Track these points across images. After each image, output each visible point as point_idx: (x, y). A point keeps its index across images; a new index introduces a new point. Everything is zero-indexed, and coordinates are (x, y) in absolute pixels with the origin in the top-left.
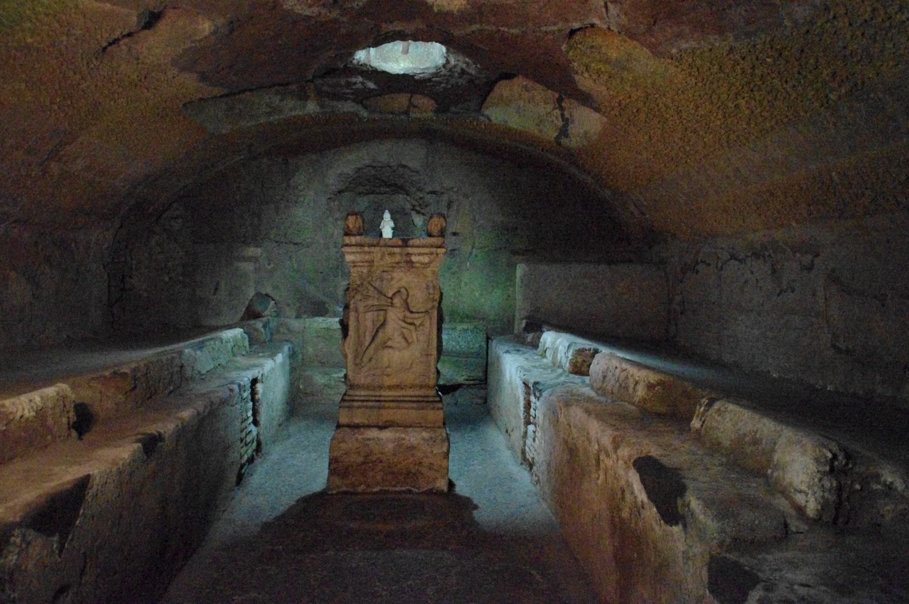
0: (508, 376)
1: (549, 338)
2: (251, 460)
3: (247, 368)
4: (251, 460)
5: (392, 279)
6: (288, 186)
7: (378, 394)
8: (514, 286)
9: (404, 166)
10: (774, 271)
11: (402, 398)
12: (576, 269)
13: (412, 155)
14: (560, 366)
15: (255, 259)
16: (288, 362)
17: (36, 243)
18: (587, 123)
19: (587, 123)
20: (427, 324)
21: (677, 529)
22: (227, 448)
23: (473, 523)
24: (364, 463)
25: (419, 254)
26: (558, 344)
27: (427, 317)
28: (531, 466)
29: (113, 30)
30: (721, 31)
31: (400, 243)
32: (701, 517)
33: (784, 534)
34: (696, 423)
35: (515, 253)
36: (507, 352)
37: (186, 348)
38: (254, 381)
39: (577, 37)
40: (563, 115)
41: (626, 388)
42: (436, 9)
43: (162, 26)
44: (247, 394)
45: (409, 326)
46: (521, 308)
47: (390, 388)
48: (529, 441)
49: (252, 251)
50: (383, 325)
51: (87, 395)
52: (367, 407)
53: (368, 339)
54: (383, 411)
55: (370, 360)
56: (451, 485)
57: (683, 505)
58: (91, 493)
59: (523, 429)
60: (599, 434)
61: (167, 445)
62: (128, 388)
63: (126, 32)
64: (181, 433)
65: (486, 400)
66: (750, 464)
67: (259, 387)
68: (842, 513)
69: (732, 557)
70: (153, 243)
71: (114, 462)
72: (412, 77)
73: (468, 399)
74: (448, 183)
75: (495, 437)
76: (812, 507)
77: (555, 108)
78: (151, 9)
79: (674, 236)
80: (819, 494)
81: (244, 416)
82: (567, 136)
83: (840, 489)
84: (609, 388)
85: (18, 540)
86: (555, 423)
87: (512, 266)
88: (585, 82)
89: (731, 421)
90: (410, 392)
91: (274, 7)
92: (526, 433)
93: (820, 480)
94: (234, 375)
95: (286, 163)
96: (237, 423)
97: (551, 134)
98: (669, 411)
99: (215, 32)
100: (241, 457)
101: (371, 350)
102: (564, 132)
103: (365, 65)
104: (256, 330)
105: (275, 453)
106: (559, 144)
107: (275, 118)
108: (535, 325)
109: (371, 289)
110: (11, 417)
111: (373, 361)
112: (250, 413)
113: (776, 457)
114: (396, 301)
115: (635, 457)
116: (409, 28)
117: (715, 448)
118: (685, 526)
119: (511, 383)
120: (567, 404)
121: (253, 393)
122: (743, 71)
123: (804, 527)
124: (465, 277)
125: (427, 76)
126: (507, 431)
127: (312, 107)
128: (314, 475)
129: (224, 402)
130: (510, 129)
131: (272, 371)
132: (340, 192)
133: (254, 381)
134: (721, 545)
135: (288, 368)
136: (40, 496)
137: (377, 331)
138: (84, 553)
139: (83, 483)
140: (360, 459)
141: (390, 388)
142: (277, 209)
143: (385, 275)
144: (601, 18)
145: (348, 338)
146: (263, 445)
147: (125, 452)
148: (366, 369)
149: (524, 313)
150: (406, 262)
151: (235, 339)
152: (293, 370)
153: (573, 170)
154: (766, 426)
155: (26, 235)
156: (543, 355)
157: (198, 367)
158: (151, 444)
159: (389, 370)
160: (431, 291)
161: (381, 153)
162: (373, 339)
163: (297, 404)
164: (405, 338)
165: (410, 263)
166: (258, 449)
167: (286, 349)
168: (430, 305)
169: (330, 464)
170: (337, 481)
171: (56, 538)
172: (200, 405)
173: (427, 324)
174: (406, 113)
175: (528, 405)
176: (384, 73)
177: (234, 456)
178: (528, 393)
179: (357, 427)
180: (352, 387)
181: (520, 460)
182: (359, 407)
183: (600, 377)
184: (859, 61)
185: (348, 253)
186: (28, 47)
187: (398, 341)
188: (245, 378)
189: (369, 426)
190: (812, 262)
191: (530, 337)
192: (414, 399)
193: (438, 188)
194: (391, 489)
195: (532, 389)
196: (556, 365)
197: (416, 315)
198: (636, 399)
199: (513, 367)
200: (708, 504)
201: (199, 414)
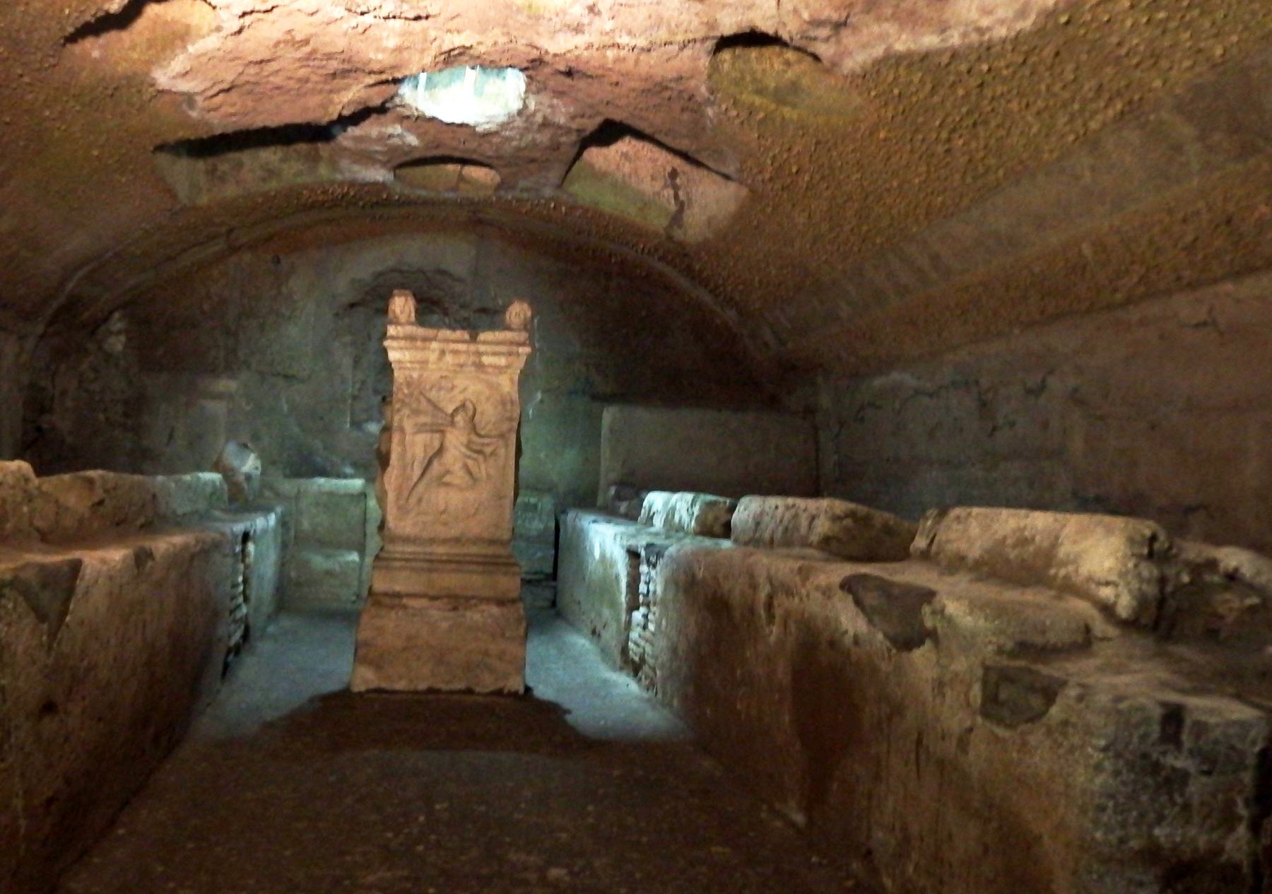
0: (597, 554)
1: (656, 500)
5: (453, 388)
6: (280, 293)
8: (598, 445)
15: (228, 397)
20: (502, 451)
24: (405, 649)
25: (495, 354)
27: (501, 442)
33: (1085, 642)
36: (594, 521)
40: (676, 196)
45: (475, 455)
46: (609, 468)
49: (226, 385)
50: (440, 451)
52: (413, 569)
53: (417, 472)
54: (435, 576)
55: (420, 501)
58: (81, 586)
70: (84, 366)
77: (665, 186)
80: (1135, 585)
82: (680, 226)
83: (1162, 581)
84: (767, 535)
92: (629, 623)
93: (1136, 566)
95: (277, 261)
101: (421, 488)
106: (670, 238)
107: (273, 185)
109: (422, 399)
111: (424, 504)
113: (1062, 552)
114: (459, 419)
123: (1112, 631)
125: (491, 127)
126: (594, 632)
130: (602, 215)
132: (352, 305)
133: (246, 537)
134: (1000, 651)
137: (430, 462)
140: (399, 643)
142: (262, 328)
148: (412, 515)
149: (613, 476)
150: (474, 364)
154: (1040, 521)
156: (650, 519)
158: (142, 557)
159: (444, 516)
160: (509, 407)
162: (423, 474)
164: (470, 473)
165: (480, 366)
166: (246, 636)
168: (505, 427)
180: (394, 539)
184: (1137, 65)
185: (394, 349)
187: (458, 476)
190: (1044, 381)
191: (623, 507)
197: (486, 441)
198: (814, 538)
199: (605, 540)
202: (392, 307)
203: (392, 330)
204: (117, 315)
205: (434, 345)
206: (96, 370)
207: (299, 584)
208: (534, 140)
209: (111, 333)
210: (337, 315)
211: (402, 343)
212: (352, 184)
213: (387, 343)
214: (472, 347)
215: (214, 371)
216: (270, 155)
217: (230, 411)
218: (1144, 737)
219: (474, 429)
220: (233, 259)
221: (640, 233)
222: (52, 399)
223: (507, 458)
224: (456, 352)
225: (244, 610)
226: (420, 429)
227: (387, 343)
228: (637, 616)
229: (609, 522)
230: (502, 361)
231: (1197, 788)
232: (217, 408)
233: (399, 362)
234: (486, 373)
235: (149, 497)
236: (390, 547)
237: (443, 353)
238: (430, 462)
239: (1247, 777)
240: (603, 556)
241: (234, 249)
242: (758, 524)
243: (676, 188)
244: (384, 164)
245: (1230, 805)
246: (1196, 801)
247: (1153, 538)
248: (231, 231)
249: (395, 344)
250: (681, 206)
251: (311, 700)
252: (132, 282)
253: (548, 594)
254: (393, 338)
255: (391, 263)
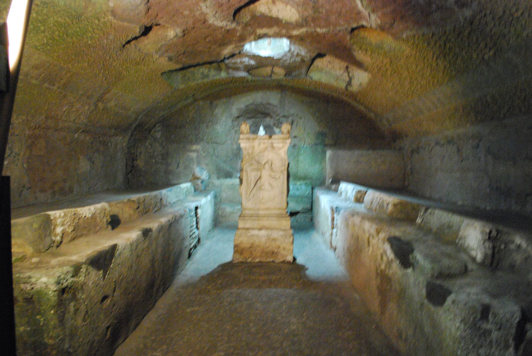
1: (343, 186)
2: (195, 247)
3: (193, 201)
4: (195, 247)
9: (270, 104)
10: (459, 150)
12: (357, 152)
13: (273, 98)
14: (349, 199)
16: (213, 200)
17: (92, 143)
18: (361, 78)
19: (361, 78)
21: (410, 270)
22: (184, 239)
23: (305, 276)
26: (348, 189)
28: (335, 249)
29: (128, 36)
30: (429, 25)
32: (422, 263)
33: (465, 271)
34: (419, 220)
35: (325, 145)
37: (164, 192)
38: (196, 208)
39: (356, 32)
41: (383, 206)
42: (284, 22)
43: (151, 34)
44: (193, 213)
47: (264, 209)
48: (334, 237)
49: (194, 147)
50: (260, 178)
51: (116, 211)
56: (295, 259)
57: (413, 259)
58: (117, 253)
60: (369, 227)
61: (154, 234)
62: (136, 207)
63: (134, 36)
64: (161, 228)
65: (312, 220)
66: (448, 239)
67: (199, 211)
68: (495, 260)
69: (438, 282)
70: (147, 144)
71: (128, 239)
72: (273, 58)
73: (303, 219)
74: (292, 111)
75: (316, 236)
76: (479, 257)
78: (146, 24)
79: (406, 136)
80: (483, 250)
81: (192, 224)
83: (494, 248)
84: (374, 207)
85: (84, 271)
86: (347, 225)
87: (324, 153)
88: (359, 55)
89: (438, 217)
91: (205, 22)
94: (187, 204)
96: (189, 229)
97: (343, 85)
98: (405, 216)
99: (176, 36)
100: (190, 245)
102: (349, 83)
103: (249, 52)
104: (197, 184)
105: (206, 244)
107: (206, 80)
108: (336, 181)
110: (80, 216)
112: (195, 223)
113: (461, 233)
115: (387, 237)
116: (271, 31)
117: (429, 231)
118: (414, 269)
119: (324, 208)
120: (353, 215)
121: (196, 214)
122: (440, 46)
124: (301, 158)
127: (223, 75)
128: (227, 255)
129: (181, 216)
131: (205, 203)
132: (238, 117)
133: (196, 208)
134: (432, 276)
135: (213, 204)
136: (94, 252)
137: (257, 182)
138: (115, 281)
139: (114, 247)
141: (264, 209)
142: (207, 126)
144: (367, 21)
145: (243, 185)
146: (201, 240)
147: (134, 235)
151: (187, 188)
152: (215, 204)
153: (354, 104)
154: (456, 219)
155: (88, 138)
157: (169, 200)
158: (146, 233)
161: (257, 98)
163: (218, 222)
167: (212, 193)
169: (234, 248)
170: (238, 256)
171: (101, 272)
172: (170, 217)
173: (282, 177)
174: (271, 76)
175: (333, 219)
176: (258, 56)
177: (187, 243)
178: (333, 214)
179: (248, 229)
181: (329, 246)
183: (370, 202)
186: (89, 45)
188: (193, 206)
189: (253, 229)
191: (334, 187)
193: (286, 114)
195: (335, 210)
196: (346, 199)
199: (325, 201)
200: (426, 256)
201: (169, 221)
202: (241, 128)
204: (157, 125)
206: (151, 145)
207: (222, 217)
208: (295, 61)
209: (156, 132)
210: (232, 121)
212: (233, 77)
215: (192, 143)
216: (204, 70)
217: (197, 156)
218: (474, 318)
219: (272, 169)
220: (196, 103)
221: (336, 90)
222: (137, 155)
223: (283, 182)
224: (264, 143)
225: (197, 233)
228: (335, 230)
229: (327, 194)
230: (281, 145)
231: (495, 335)
232: (194, 155)
235: (159, 200)
236: (244, 212)
237: (260, 144)
239: (514, 331)
240: (324, 206)
241: (196, 100)
242: (372, 203)
243: (349, 73)
244: (244, 70)
245: (507, 341)
246: (494, 339)
247: (490, 232)
248: (194, 95)
250: (350, 79)
251: (219, 267)
252: (161, 114)
253: (310, 216)
255: (251, 101)
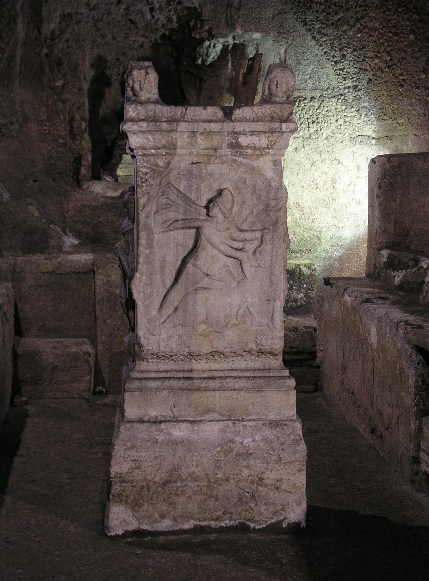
7: (186, 367)
11: (226, 374)
25: (253, 133)
31: (220, 114)
52: (171, 390)
59: (413, 425)
90: (240, 363)
143: (195, 169)
165: (235, 147)
179: (156, 422)
182: (158, 389)
189: (176, 420)
192: (248, 374)
194: (213, 524)
203: (131, 111)
205: (183, 126)
211: (144, 125)
213: (127, 127)
214: (228, 127)
224: (207, 134)
226: (170, 226)
227: (127, 127)
233: (143, 148)
234: (246, 156)
238: (184, 262)
249: (135, 128)
254: (133, 120)
